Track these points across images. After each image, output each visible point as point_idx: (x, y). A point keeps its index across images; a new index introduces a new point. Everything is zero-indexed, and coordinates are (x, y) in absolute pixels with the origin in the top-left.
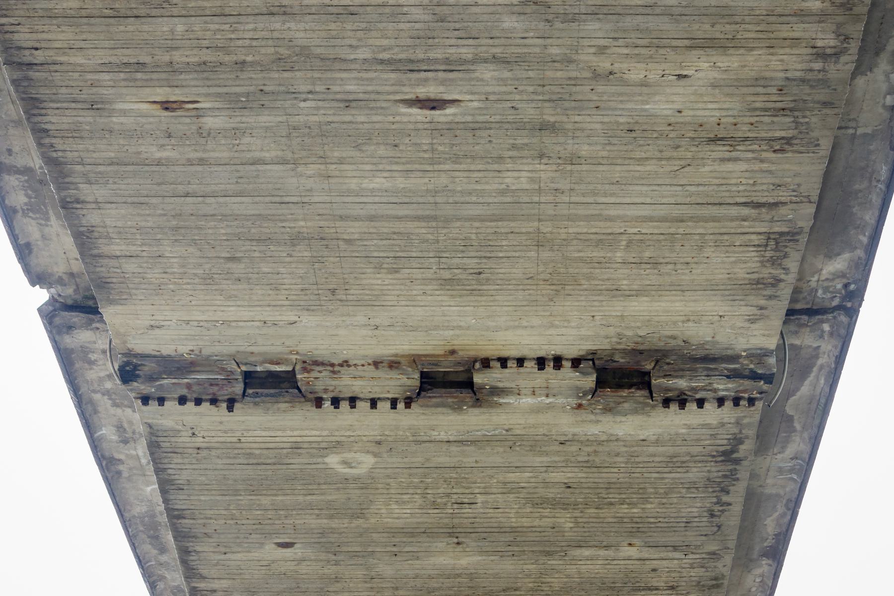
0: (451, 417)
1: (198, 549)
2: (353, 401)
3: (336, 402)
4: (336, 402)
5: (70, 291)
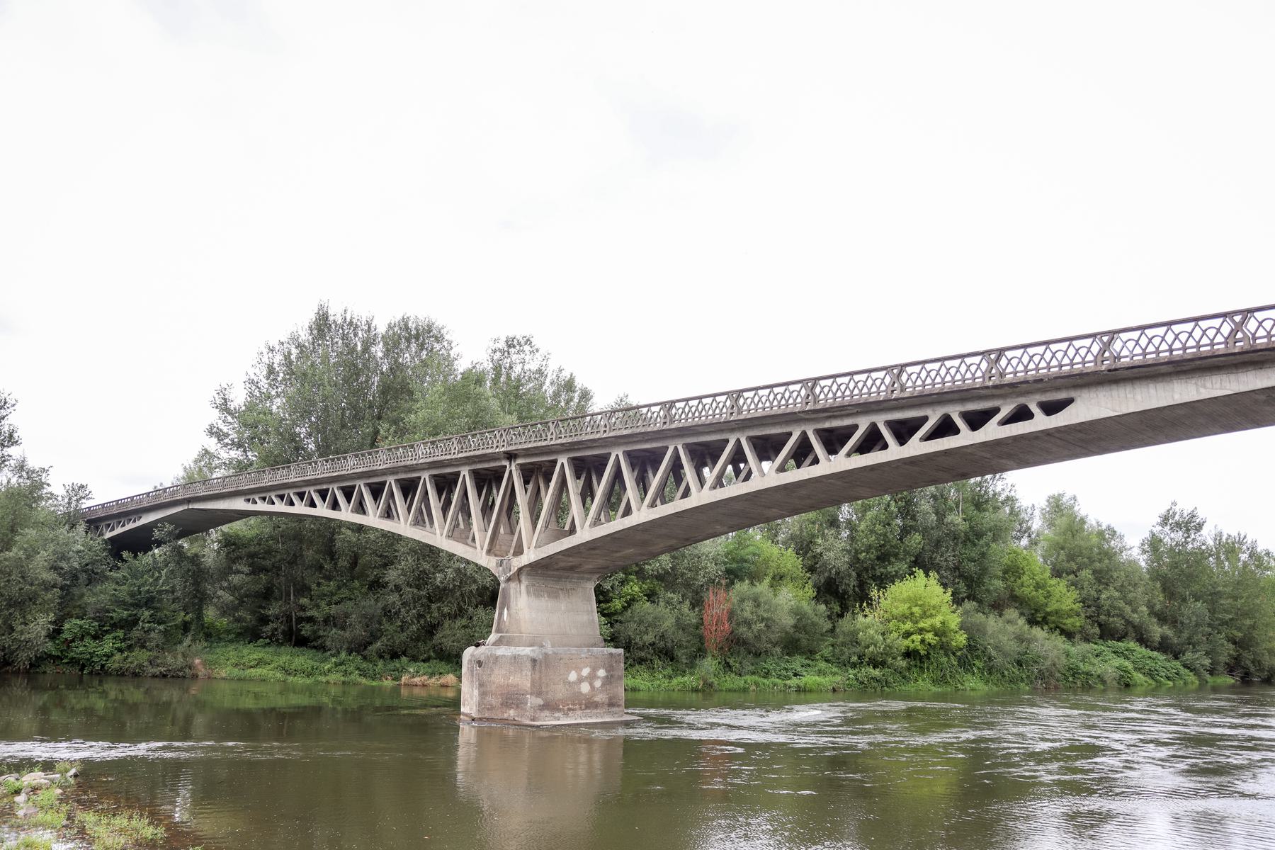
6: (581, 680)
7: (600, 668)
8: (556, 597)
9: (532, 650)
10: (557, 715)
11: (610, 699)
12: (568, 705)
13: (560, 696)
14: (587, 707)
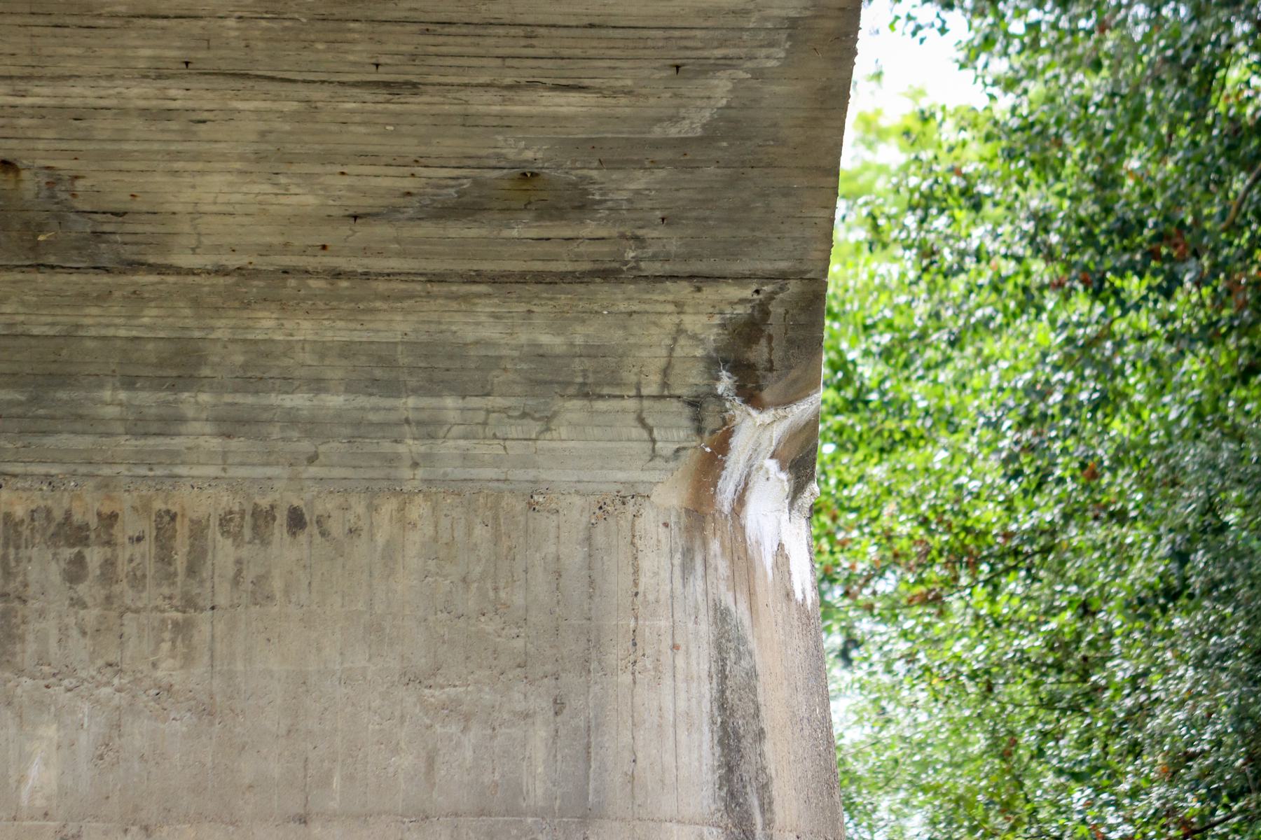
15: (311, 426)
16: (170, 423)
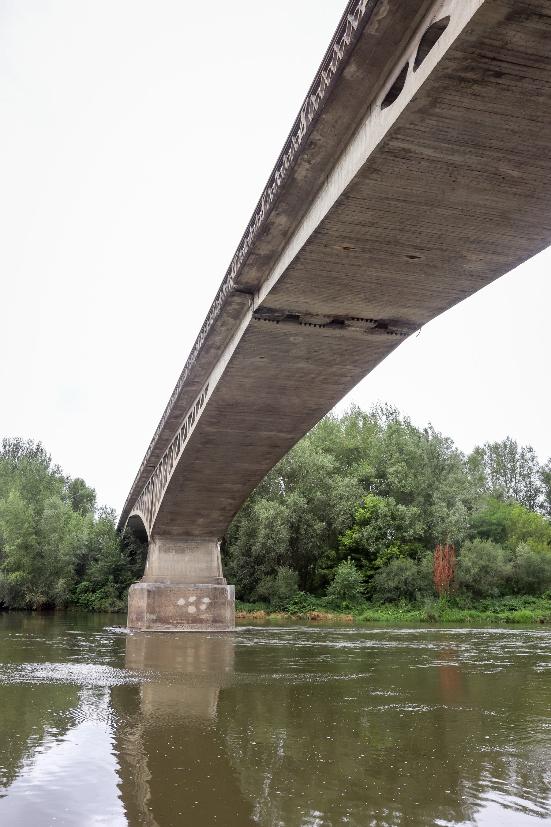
0: (331, 331)
1: (238, 357)
2: (310, 324)
3: (305, 324)
4: (305, 324)
5: (242, 287)
6: (188, 604)
7: (205, 597)
8: (182, 553)
9: (148, 585)
10: (167, 626)
11: (214, 617)
12: (177, 620)
13: (170, 614)
14: (193, 622)
15: (198, 543)
16: (192, 543)
